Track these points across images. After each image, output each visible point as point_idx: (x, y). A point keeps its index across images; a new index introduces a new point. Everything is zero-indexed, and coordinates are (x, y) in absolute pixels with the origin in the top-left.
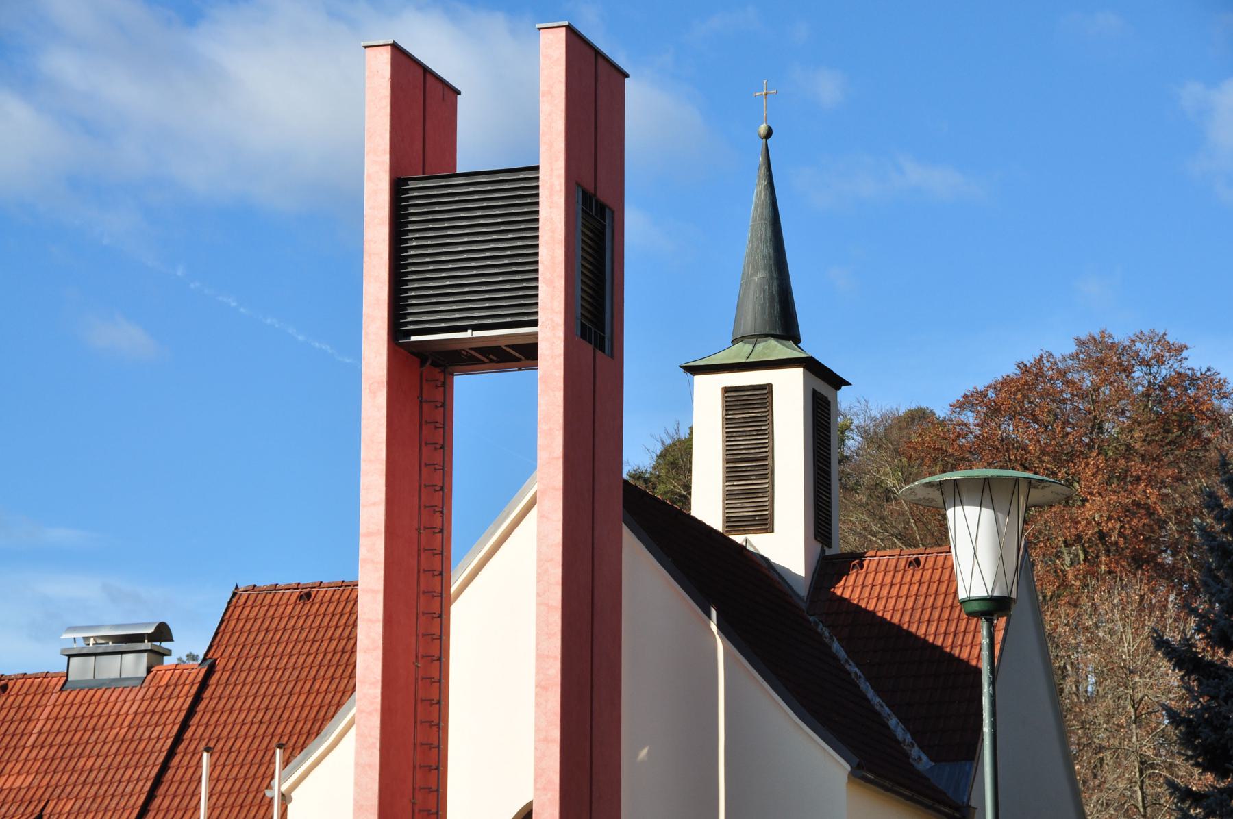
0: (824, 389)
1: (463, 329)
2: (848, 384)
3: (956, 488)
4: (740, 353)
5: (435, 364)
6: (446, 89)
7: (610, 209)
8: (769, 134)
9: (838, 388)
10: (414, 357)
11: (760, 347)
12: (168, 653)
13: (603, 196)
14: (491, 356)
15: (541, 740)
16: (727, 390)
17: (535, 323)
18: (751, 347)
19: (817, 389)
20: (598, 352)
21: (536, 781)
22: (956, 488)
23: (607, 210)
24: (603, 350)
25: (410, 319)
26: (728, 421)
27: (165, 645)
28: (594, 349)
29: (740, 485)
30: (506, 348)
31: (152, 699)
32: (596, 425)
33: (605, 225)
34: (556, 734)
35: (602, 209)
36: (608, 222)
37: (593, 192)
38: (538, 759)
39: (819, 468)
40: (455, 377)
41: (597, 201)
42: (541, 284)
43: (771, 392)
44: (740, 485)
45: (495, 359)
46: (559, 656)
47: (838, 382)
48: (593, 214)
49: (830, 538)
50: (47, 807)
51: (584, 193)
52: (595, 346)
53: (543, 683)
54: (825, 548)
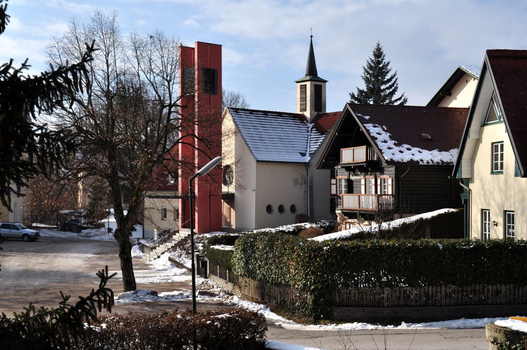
8: (312, 37)
16: (301, 86)
47: (325, 81)
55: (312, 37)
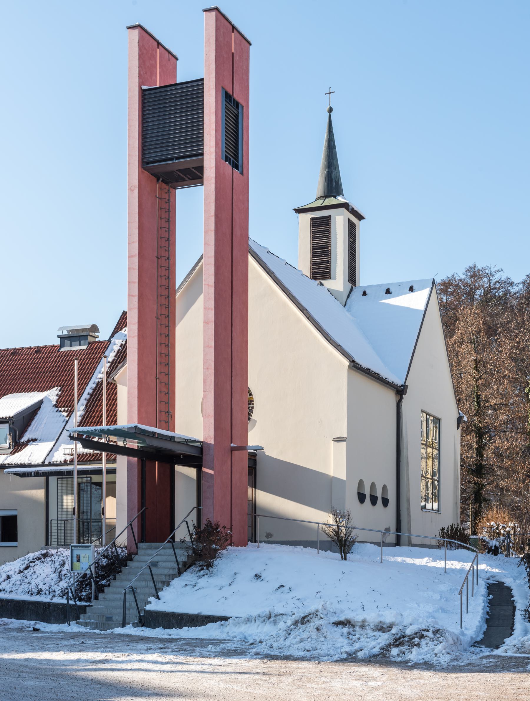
0: (354, 220)
1: (172, 159)
2: (363, 218)
3: (466, 584)
4: (319, 203)
5: (164, 182)
6: (170, 55)
7: (241, 105)
8: (331, 110)
9: (360, 220)
10: (153, 177)
11: (326, 200)
12: (98, 337)
13: (237, 96)
14: (188, 176)
15: (206, 347)
16: (312, 219)
17: (202, 154)
18: (323, 201)
19: (351, 219)
20: (235, 170)
21: (204, 366)
22: (466, 584)
23: (240, 105)
24: (237, 169)
25: (149, 156)
26: (313, 232)
27: (96, 334)
28: (232, 169)
29: (318, 260)
30: (193, 170)
31: (90, 354)
32: (234, 205)
33: (238, 112)
34: (212, 344)
35: (237, 105)
36: (240, 111)
37: (232, 94)
38: (205, 355)
39: (351, 252)
40: (178, 191)
41: (234, 99)
42: (205, 135)
43: (330, 219)
44: (318, 260)
45: (190, 177)
46: (213, 308)
47: (360, 217)
48: (232, 105)
49: (356, 283)
50: (401, 459)
51: (227, 94)
52: (233, 167)
53: (206, 321)
54: (353, 286)
55: (331, 110)
